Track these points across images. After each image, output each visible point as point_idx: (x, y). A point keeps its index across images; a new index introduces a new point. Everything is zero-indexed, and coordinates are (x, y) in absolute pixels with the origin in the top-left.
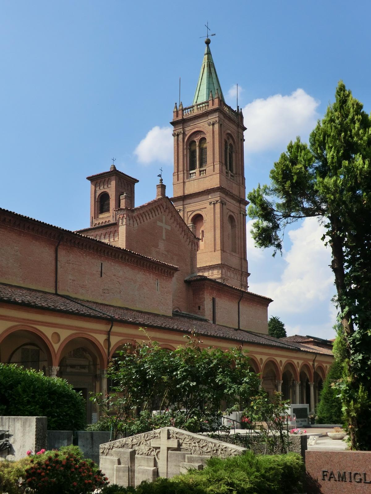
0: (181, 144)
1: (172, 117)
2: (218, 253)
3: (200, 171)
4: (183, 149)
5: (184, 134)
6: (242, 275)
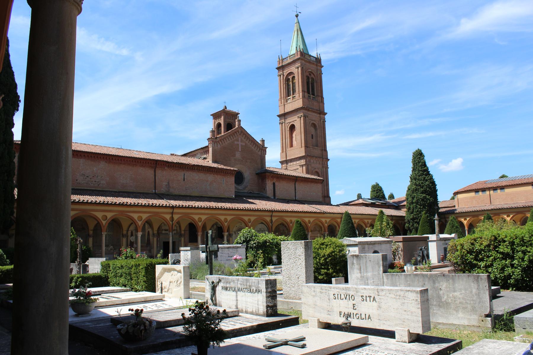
0: (282, 81)
2: (303, 149)
3: (293, 97)
5: (283, 76)
6: (323, 160)
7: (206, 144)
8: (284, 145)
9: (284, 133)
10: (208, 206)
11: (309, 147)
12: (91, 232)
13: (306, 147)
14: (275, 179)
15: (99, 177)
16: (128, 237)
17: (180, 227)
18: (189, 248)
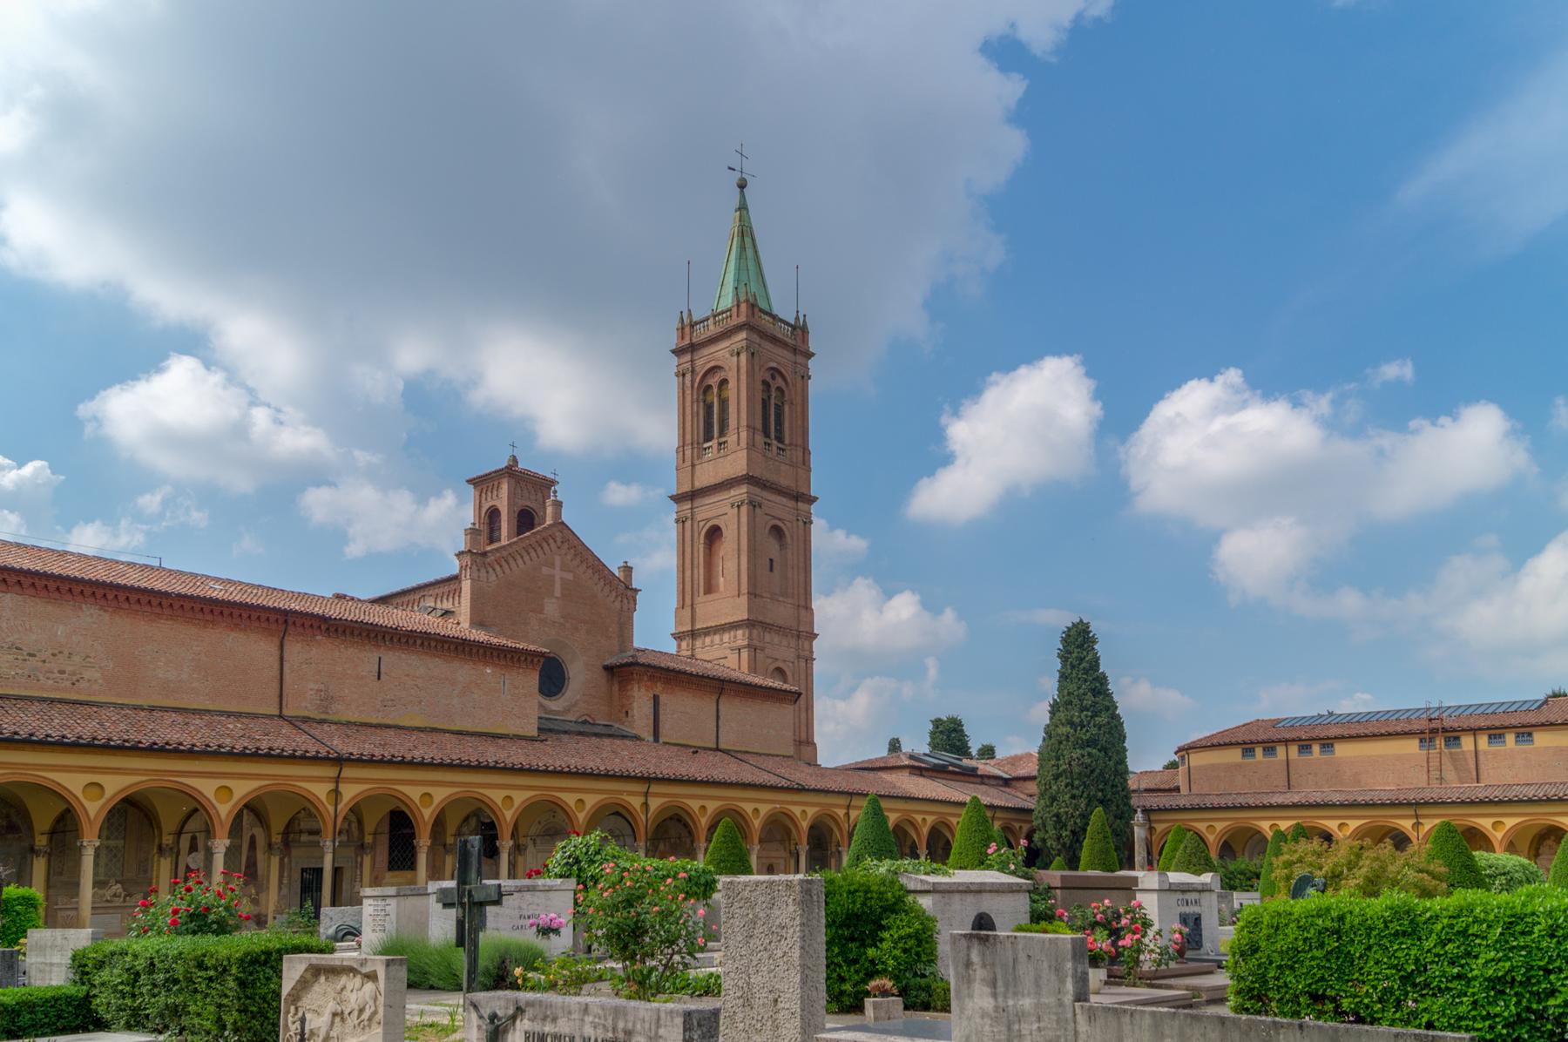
0: (688, 392)
1: (673, 341)
2: (744, 599)
3: (720, 444)
4: (692, 402)
7: (453, 567)
8: (688, 588)
9: (688, 550)
10: (454, 758)
11: (762, 597)
12: (41, 841)
13: (753, 594)
14: (659, 684)
15: (77, 659)
16: (178, 854)
17: (360, 822)
18: (392, 891)
